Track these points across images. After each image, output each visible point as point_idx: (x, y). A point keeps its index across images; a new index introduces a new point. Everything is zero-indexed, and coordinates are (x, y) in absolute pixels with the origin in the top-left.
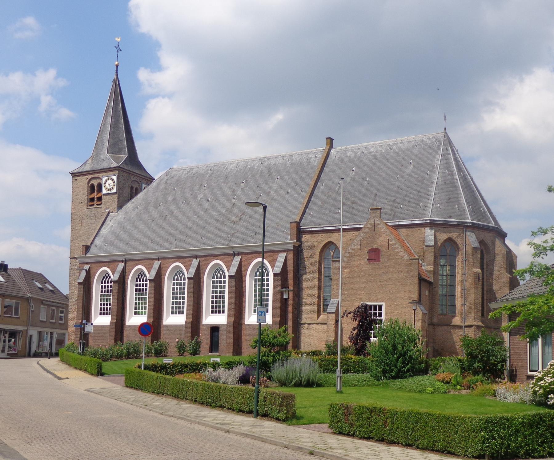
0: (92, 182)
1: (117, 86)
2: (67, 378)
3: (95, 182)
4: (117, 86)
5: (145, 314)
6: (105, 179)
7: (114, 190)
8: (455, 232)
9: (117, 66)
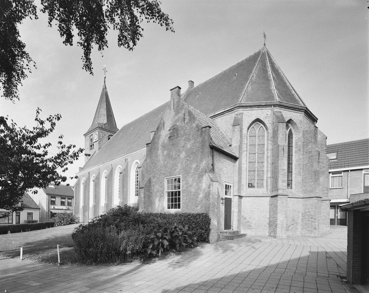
3: (91, 137)
6: (94, 135)
9: (105, 78)
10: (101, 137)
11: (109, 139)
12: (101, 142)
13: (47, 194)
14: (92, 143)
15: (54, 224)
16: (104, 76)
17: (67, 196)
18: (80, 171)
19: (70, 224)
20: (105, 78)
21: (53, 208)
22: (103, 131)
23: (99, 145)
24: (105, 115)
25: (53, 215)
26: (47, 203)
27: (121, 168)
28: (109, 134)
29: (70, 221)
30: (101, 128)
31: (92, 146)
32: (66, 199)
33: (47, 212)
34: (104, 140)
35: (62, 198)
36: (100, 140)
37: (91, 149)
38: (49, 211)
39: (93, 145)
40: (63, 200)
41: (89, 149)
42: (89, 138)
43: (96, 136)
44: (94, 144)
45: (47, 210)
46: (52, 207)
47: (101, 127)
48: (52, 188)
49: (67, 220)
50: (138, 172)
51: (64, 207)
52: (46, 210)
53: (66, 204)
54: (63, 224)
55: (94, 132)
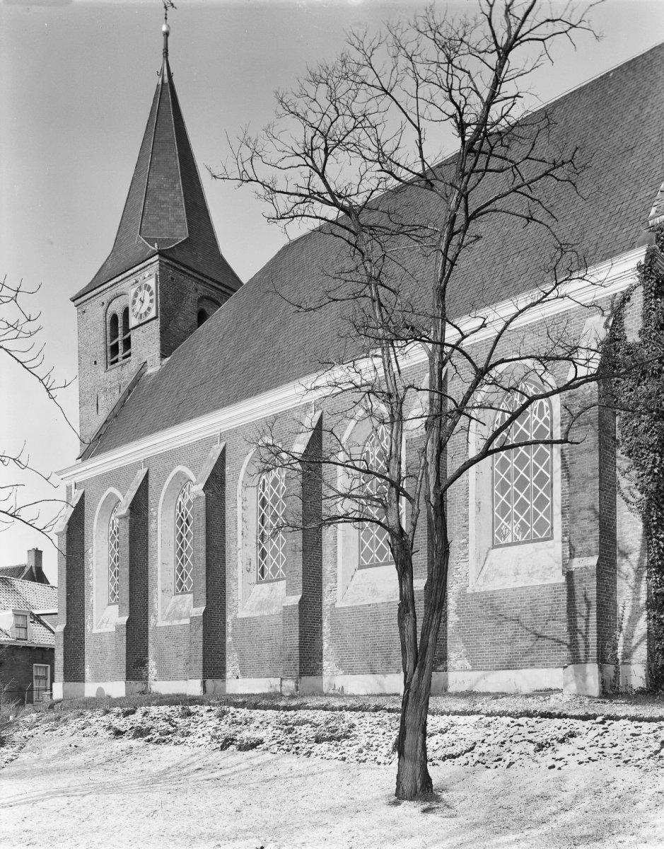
0: (111, 310)
3: (117, 308)
9: (167, 34)
16: (164, 28)
20: (167, 34)
31: (121, 347)
42: (101, 310)
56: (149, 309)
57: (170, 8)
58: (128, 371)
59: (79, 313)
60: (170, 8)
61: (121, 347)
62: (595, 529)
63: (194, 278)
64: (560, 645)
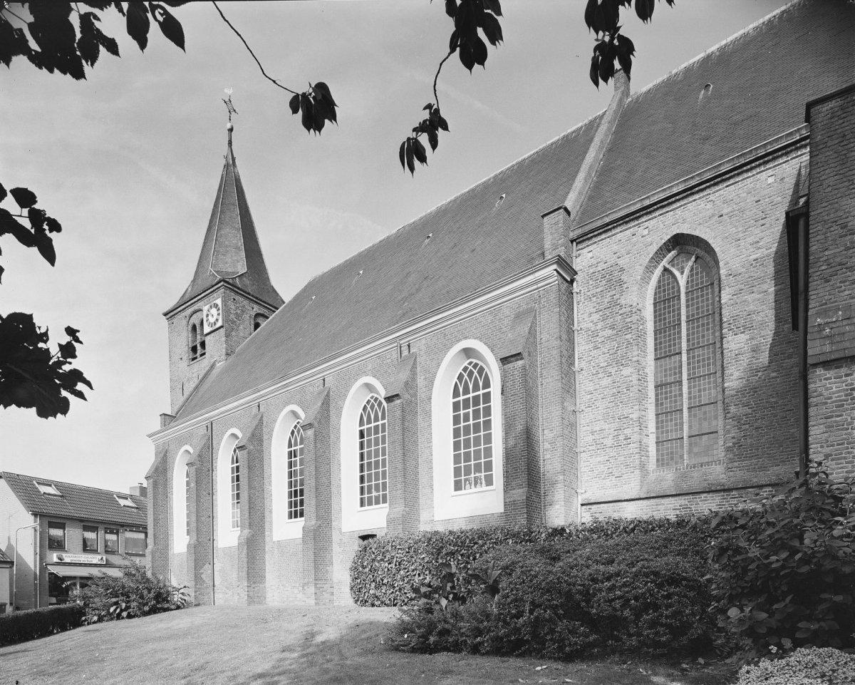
0: (192, 321)
1: (230, 165)
2: (9, 538)
3: (195, 320)
4: (230, 165)
5: (385, 501)
6: (205, 308)
7: (219, 324)
8: (323, 643)
9: (231, 130)
10: (232, 316)
11: (257, 326)
12: (233, 333)
13: (35, 515)
14: (199, 337)
15: (84, 615)
16: (229, 126)
17: (102, 522)
18: (164, 424)
19: (154, 611)
20: (231, 130)
21: (56, 560)
22: (237, 297)
23: (226, 342)
24: (238, 248)
25: (58, 586)
26: (35, 544)
27: (192, 451)
28: (257, 309)
29: (153, 602)
30: (230, 285)
31: (199, 347)
32: (101, 533)
33: (35, 574)
34: (241, 327)
35: (86, 528)
36: (229, 326)
37: (193, 359)
38: (43, 569)
39: (203, 344)
40: (90, 535)
41: (185, 358)
42: (184, 322)
43: (214, 311)
44: (207, 339)
45: (35, 566)
46: (54, 557)
47: (231, 281)
48: (49, 494)
49: (142, 597)
50: (237, 462)
51: (95, 559)
52: (32, 566)
53: (101, 548)
54: (125, 614)
55: (206, 300)
56: (217, 320)
57: (233, 113)
58: (203, 364)
59: (169, 324)
60: (233, 113)
61: (199, 347)
62: (761, 280)
63: (251, 289)
64: (675, 506)
